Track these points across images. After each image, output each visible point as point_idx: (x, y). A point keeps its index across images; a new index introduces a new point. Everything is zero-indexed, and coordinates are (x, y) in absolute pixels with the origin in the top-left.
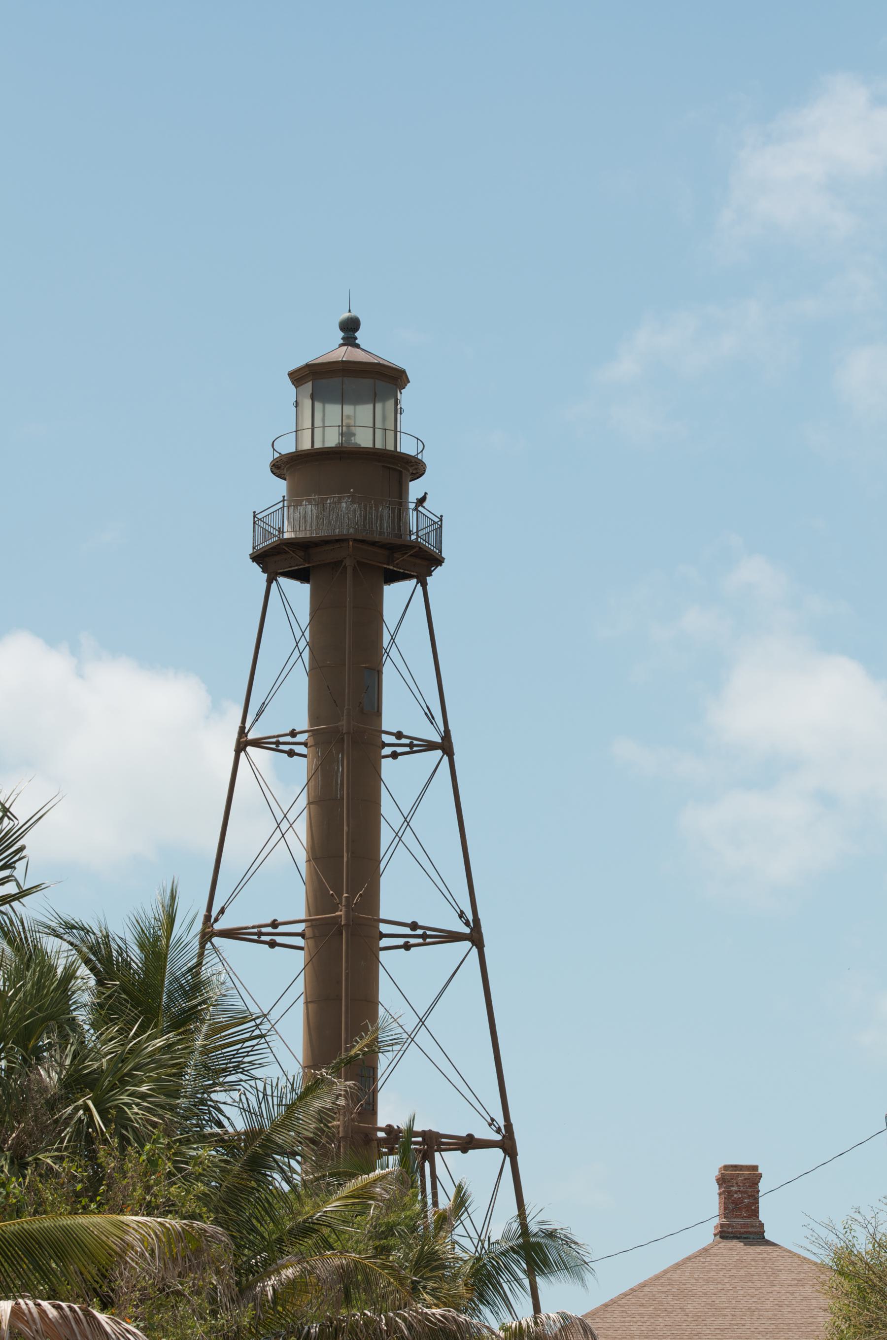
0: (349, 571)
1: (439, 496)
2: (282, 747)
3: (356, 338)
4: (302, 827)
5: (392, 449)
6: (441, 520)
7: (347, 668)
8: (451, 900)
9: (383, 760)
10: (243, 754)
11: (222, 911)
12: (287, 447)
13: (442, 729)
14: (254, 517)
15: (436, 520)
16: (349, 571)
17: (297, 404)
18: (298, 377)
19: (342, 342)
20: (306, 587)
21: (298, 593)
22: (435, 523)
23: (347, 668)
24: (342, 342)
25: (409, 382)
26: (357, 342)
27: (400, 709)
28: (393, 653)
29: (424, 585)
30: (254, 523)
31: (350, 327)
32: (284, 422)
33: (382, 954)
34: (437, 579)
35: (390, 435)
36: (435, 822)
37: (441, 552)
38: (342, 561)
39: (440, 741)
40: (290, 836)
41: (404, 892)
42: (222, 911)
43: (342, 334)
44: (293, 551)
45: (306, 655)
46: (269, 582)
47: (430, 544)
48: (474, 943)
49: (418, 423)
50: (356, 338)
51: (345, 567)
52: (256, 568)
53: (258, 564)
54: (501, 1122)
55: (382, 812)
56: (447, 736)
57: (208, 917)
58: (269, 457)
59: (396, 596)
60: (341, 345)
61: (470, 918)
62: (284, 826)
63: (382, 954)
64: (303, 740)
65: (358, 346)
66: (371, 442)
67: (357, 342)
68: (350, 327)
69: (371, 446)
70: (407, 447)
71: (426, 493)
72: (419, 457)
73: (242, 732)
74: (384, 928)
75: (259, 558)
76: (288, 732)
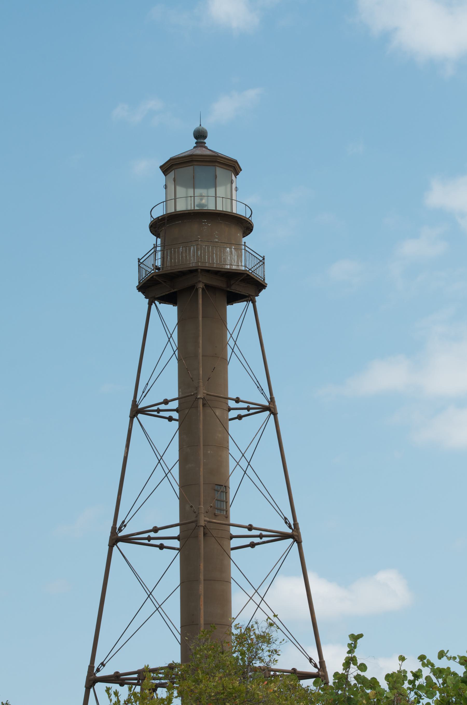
0: (200, 291)
1: (261, 248)
2: (162, 414)
3: (205, 143)
6: (264, 259)
7: (201, 360)
8: (280, 512)
9: (230, 422)
10: (135, 419)
12: (159, 212)
13: (269, 397)
14: (139, 261)
15: (261, 259)
16: (200, 291)
17: (166, 187)
18: (167, 168)
20: (176, 308)
21: (170, 312)
22: (261, 261)
23: (201, 360)
25: (241, 170)
26: (205, 145)
27: (240, 384)
28: (175, 348)
29: (254, 303)
30: (139, 265)
31: (200, 135)
32: (154, 196)
33: (233, 553)
34: (262, 298)
36: (266, 460)
37: (264, 280)
38: (195, 286)
39: (251, 302)
41: (247, 507)
42: (103, 664)
43: (196, 141)
44: (165, 282)
46: (150, 304)
47: (258, 274)
48: (295, 540)
50: (205, 143)
51: (197, 290)
52: (141, 296)
53: (143, 293)
54: (317, 660)
55: (180, 646)
57: (114, 528)
58: (148, 221)
59: (234, 311)
60: (194, 147)
61: (292, 523)
62: (257, 599)
63: (233, 553)
65: (206, 148)
66: (214, 206)
67: (205, 145)
68: (200, 135)
69: (214, 209)
70: (239, 210)
72: (250, 219)
73: (135, 404)
74: (234, 531)
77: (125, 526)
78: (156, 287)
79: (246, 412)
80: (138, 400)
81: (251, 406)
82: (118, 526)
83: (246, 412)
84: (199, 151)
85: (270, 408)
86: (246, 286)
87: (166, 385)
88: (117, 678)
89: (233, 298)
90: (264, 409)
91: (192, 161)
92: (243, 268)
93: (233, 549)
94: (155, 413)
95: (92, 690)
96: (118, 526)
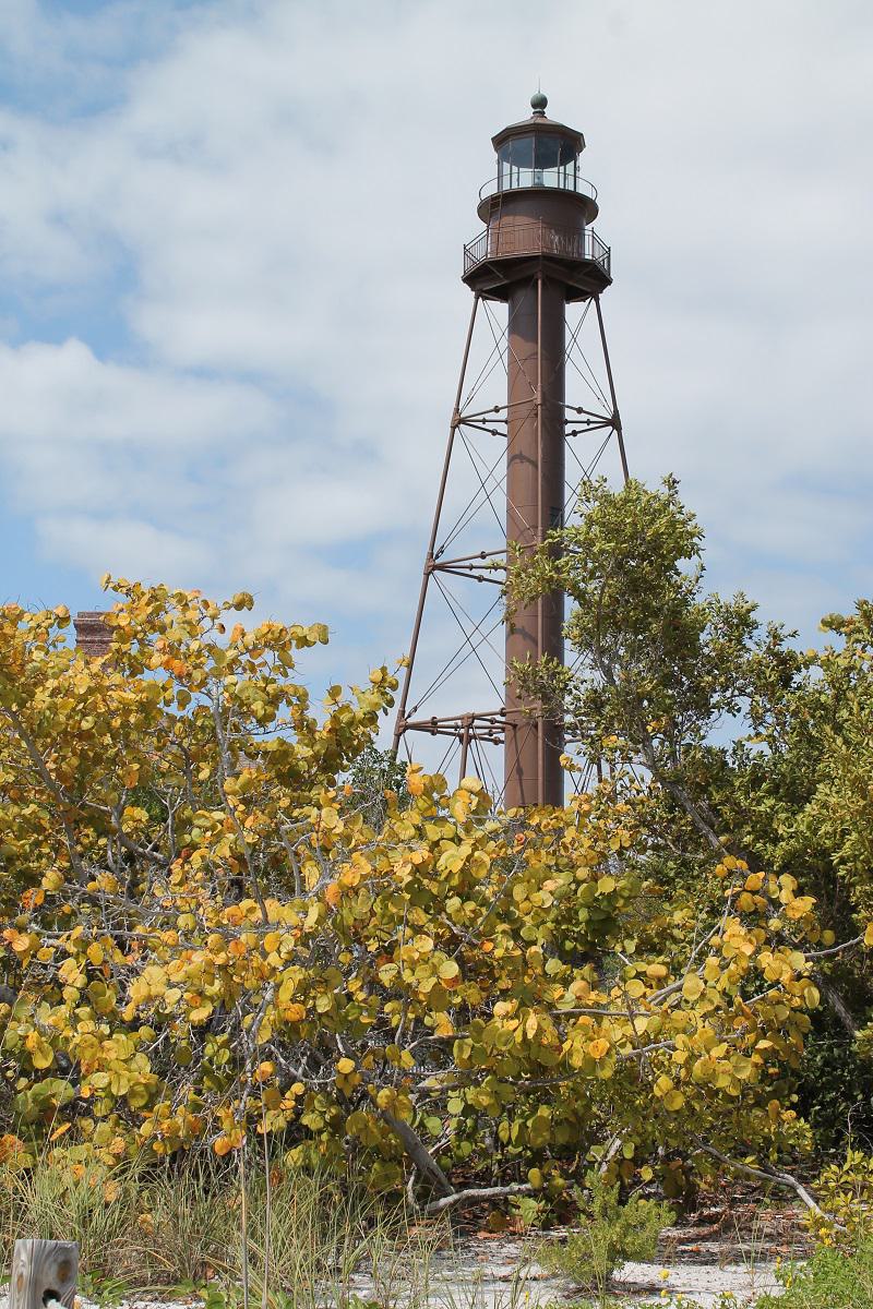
1: (605, 234)
4: (501, 500)
5: (572, 189)
10: (457, 429)
11: (415, 709)
12: (492, 190)
18: (500, 141)
19: (849, 612)
20: (505, 306)
21: (500, 310)
24: (849, 612)
31: (540, 104)
32: (484, 174)
35: (571, 179)
40: (483, 650)
42: (415, 709)
45: (505, 357)
46: (477, 298)
49: (590, 174)
56: (616, 413)
59: (573, 311)
62: (475, 639)
64: (504, 418)
68: (540, 104)
71: (824, 623)
75: (470, 279)
76: (492, 408)
77: (442, 552)
78: (487, 279)
79: (585, 426)
80: (460, 408)
81: (480, 424)
82: (435, 553)
83: (585, 426)
84: (540, 121)
85: (614, 422)
86: (590, 279)
87: (492, 389)
88: (432, 727)
89: (577, 295)
90: (608, 423)
91: (508, 136)
92: (590, 258)
93: (500, 583)
94: (480, 424)
95: (402, 737)
96: (435, 553)
